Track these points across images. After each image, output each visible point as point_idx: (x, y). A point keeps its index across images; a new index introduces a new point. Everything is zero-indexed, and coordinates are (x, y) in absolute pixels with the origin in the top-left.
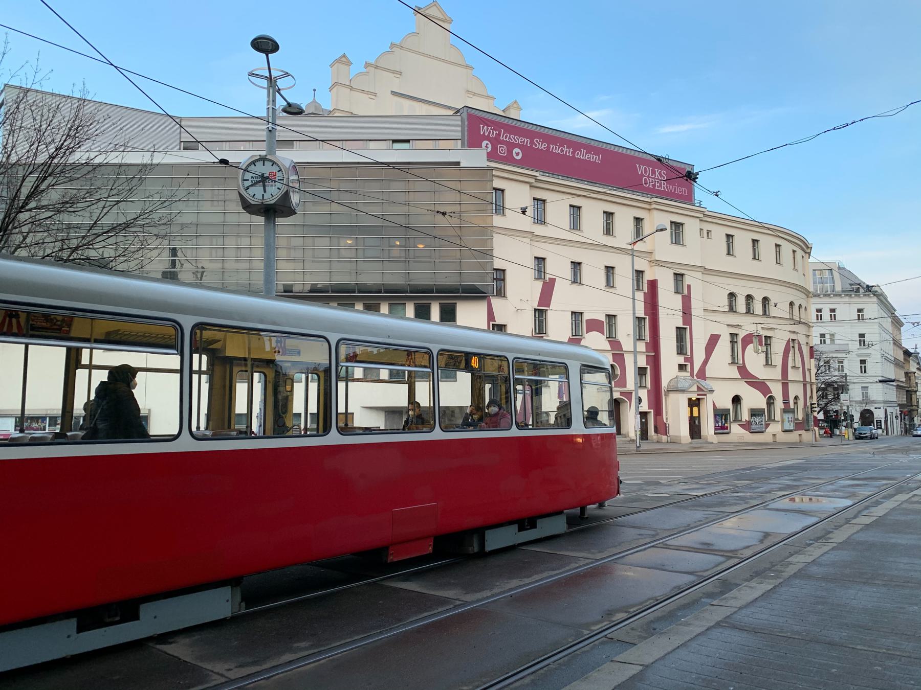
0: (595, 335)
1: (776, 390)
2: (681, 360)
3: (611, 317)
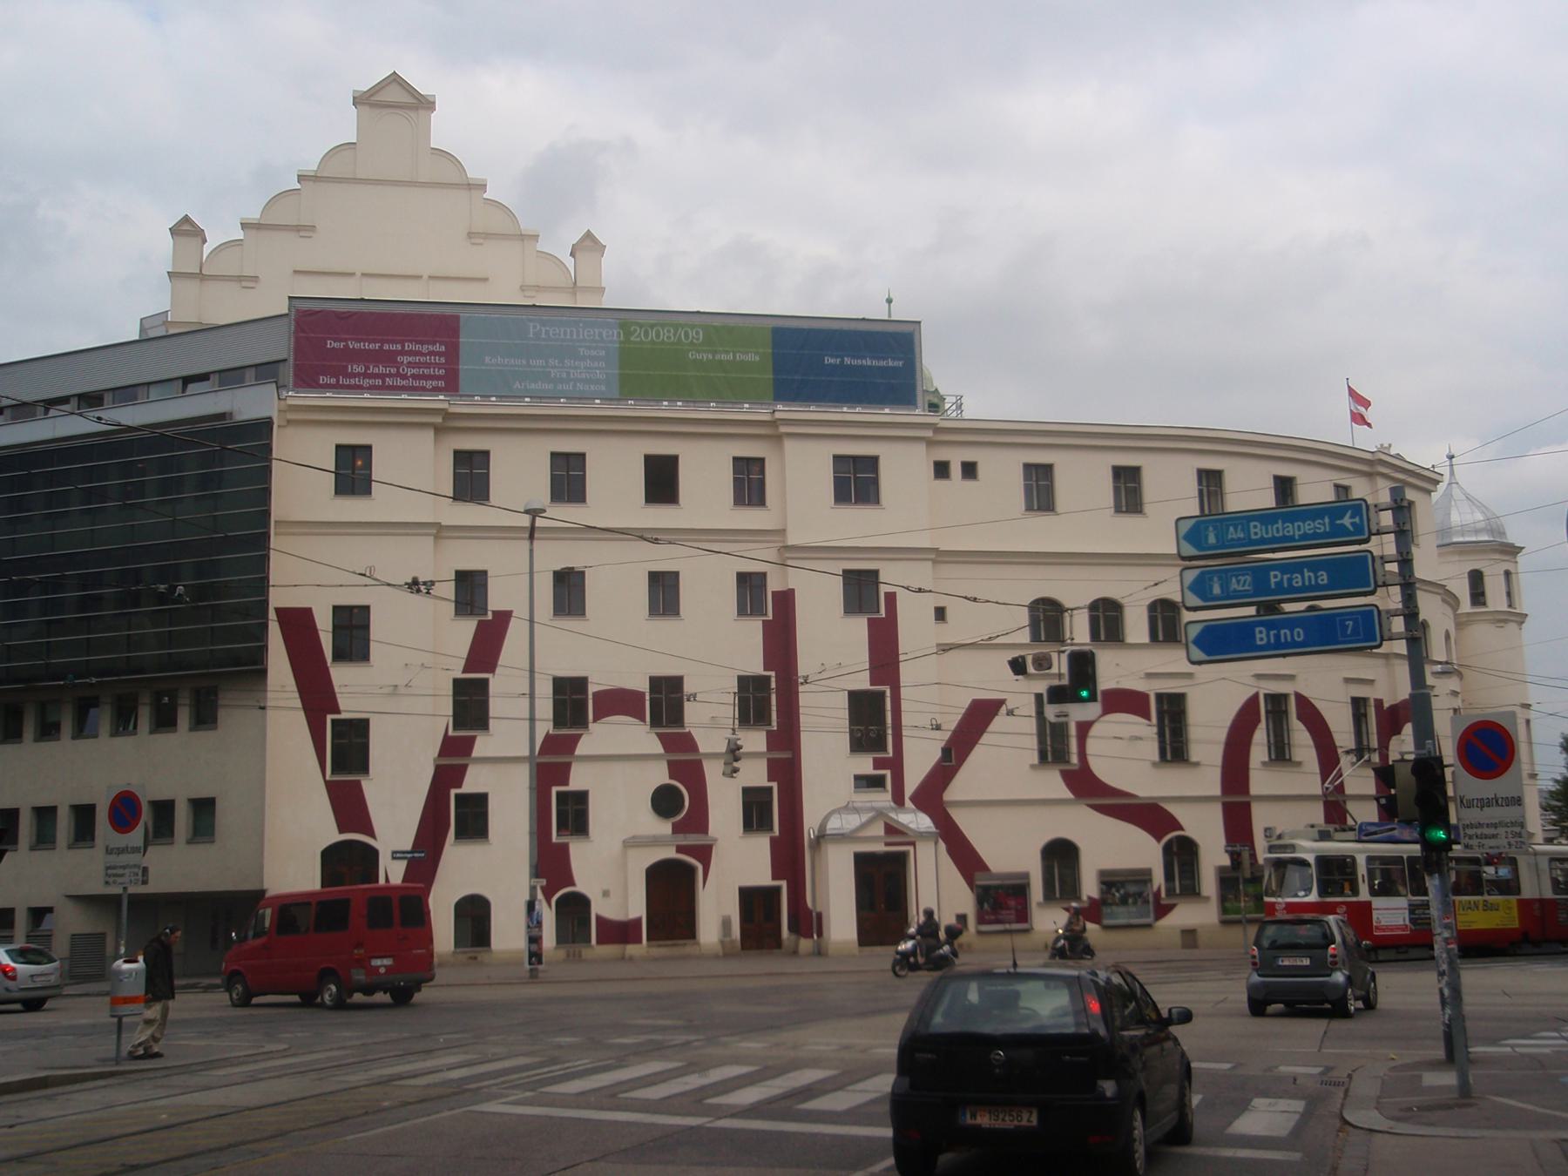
1: (1206, 830)
2: (865, 764)
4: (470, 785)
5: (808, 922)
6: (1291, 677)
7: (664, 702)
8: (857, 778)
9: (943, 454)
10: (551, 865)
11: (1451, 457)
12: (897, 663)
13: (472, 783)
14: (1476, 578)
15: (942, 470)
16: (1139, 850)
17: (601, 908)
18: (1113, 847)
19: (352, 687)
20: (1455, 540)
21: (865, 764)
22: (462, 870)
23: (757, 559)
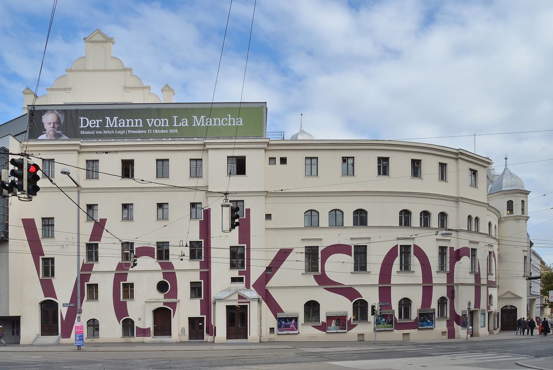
1: (372, 297)
4: (92, 281)
5: (212, 331)
7: (162, 252)
9: (272, 155)
10: (120, 310)
11: (506, 159)
12: (380, 275)
13: (93, 280)
14: (510, 205)
15: (272, 160)
16: (345, 306)
17: (137, 324)
18: (334, 304)
19: (49, 248)
20: (503, 189)
21: (235, 273)
22: (89, 310)
23: (198, 197)
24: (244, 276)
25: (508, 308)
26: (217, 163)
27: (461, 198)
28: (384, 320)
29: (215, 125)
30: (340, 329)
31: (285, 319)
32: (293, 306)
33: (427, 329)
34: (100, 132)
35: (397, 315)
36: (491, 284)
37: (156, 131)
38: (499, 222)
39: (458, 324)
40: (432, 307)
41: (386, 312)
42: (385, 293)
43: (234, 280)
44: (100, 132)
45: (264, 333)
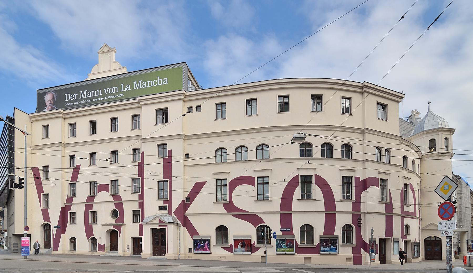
0: (104, 193)
1: (274, 224)
3: (114, 182)
6: (314, 169)
8: (159, 207)
9: (189, 104)
10: (89, 231)
11: (429, 103)
14: (432, 144)
16: (248, 231)
17: (99, 242)
18: (241, 229)
24: (167, 205)
25: (432, 239)
26: (148, 114)
27: (367, 129)
28: (285, 244)
29: (149, 86)
30: (246, 251)
31: (200, 241)
32: (207, 229)
33: (330, 254)
34: (77, 103)
35: (298, 239)
36: (405, 215)
37: (110, 97)
38: (421, 159)
39: (366, 250)
40: (336, 233)
41: (288, 237)
42: (286, 220)
43: (161, 208)
44: (77, 103)
45: (182, 252)
